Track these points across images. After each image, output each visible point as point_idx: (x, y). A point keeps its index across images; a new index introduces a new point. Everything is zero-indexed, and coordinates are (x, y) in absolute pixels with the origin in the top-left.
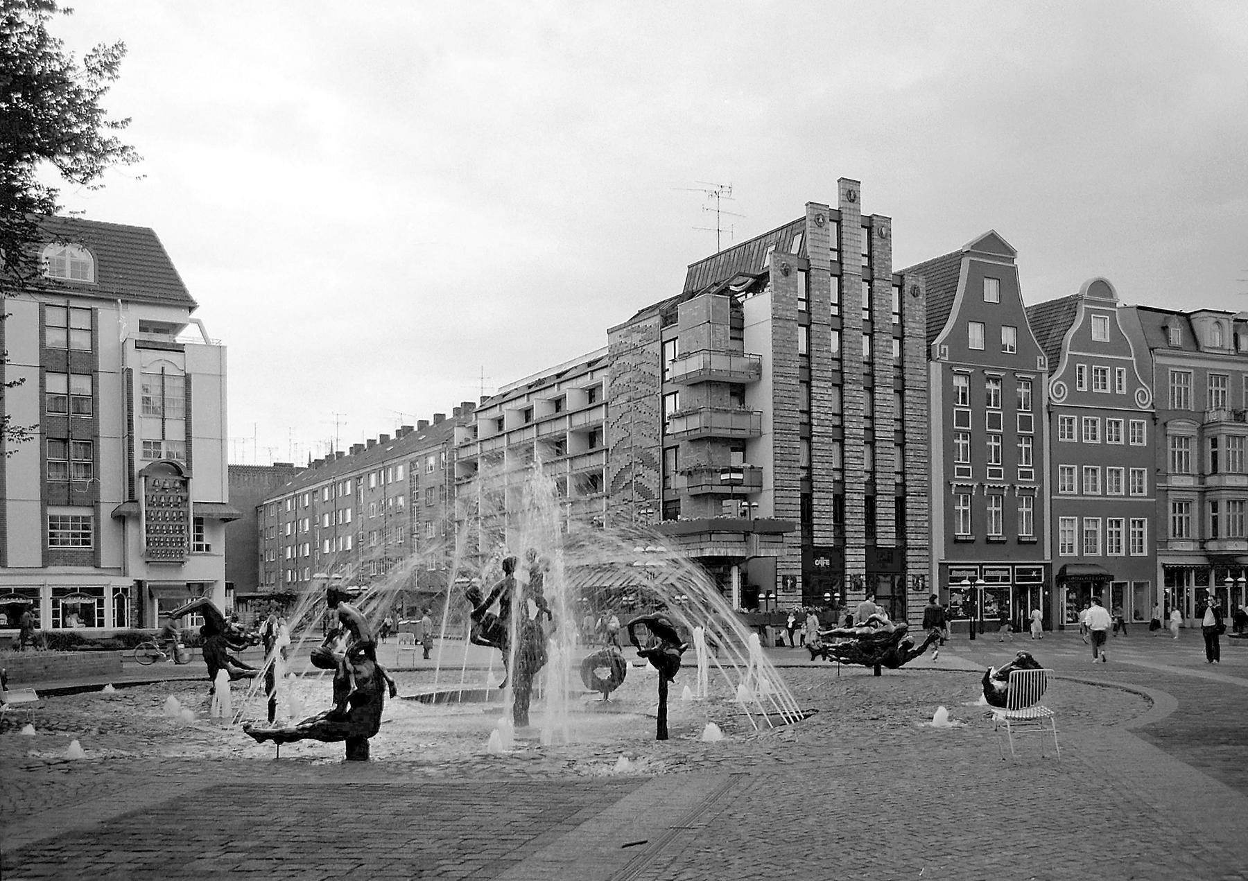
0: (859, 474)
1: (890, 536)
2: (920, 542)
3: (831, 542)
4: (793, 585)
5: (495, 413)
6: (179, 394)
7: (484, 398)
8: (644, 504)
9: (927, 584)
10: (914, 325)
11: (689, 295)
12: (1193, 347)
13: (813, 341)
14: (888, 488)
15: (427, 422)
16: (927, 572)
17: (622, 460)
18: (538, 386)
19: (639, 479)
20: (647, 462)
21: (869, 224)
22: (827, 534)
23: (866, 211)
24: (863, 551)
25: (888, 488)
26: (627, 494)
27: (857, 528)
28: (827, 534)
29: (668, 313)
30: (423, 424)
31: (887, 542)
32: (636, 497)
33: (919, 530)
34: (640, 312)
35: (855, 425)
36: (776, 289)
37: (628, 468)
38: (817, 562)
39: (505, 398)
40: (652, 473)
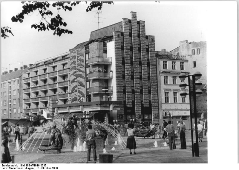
0: (139, 88)
1: (147, 104)
2: (156, 105)
3: (131, 105)
4: (122, 117)
5: (36, 69)
6: (34, 78)
7: (31, 65)
8: (81, 96)
9: (158, 116)
10: (152, 48)
11: (91, 42)
12: (42, 145)
13: (110, 27)
14: (146, 91)
15: (12, 71)
16: (157, 113)
17: (74, 84)
18: (46, 63)
19: (79, 89)
20: (81, 84)
21: (138, 22)
22: (130, 104)
23: (138, 20)
24: (140, 108)
25: (146, 91)
26: (76, 93)
27: (139, 102)
28: (130, 104)
29: (86, 45)
30: (11, 71)
31: (146, 105)
32: (79, 94)
33: (155, 102)
34: (78, 45)
35: (137, 75)
36: (115, 40)
37: (76, 87)
38: (128, 111)
39: (38, 65)
40: (83, 88)
